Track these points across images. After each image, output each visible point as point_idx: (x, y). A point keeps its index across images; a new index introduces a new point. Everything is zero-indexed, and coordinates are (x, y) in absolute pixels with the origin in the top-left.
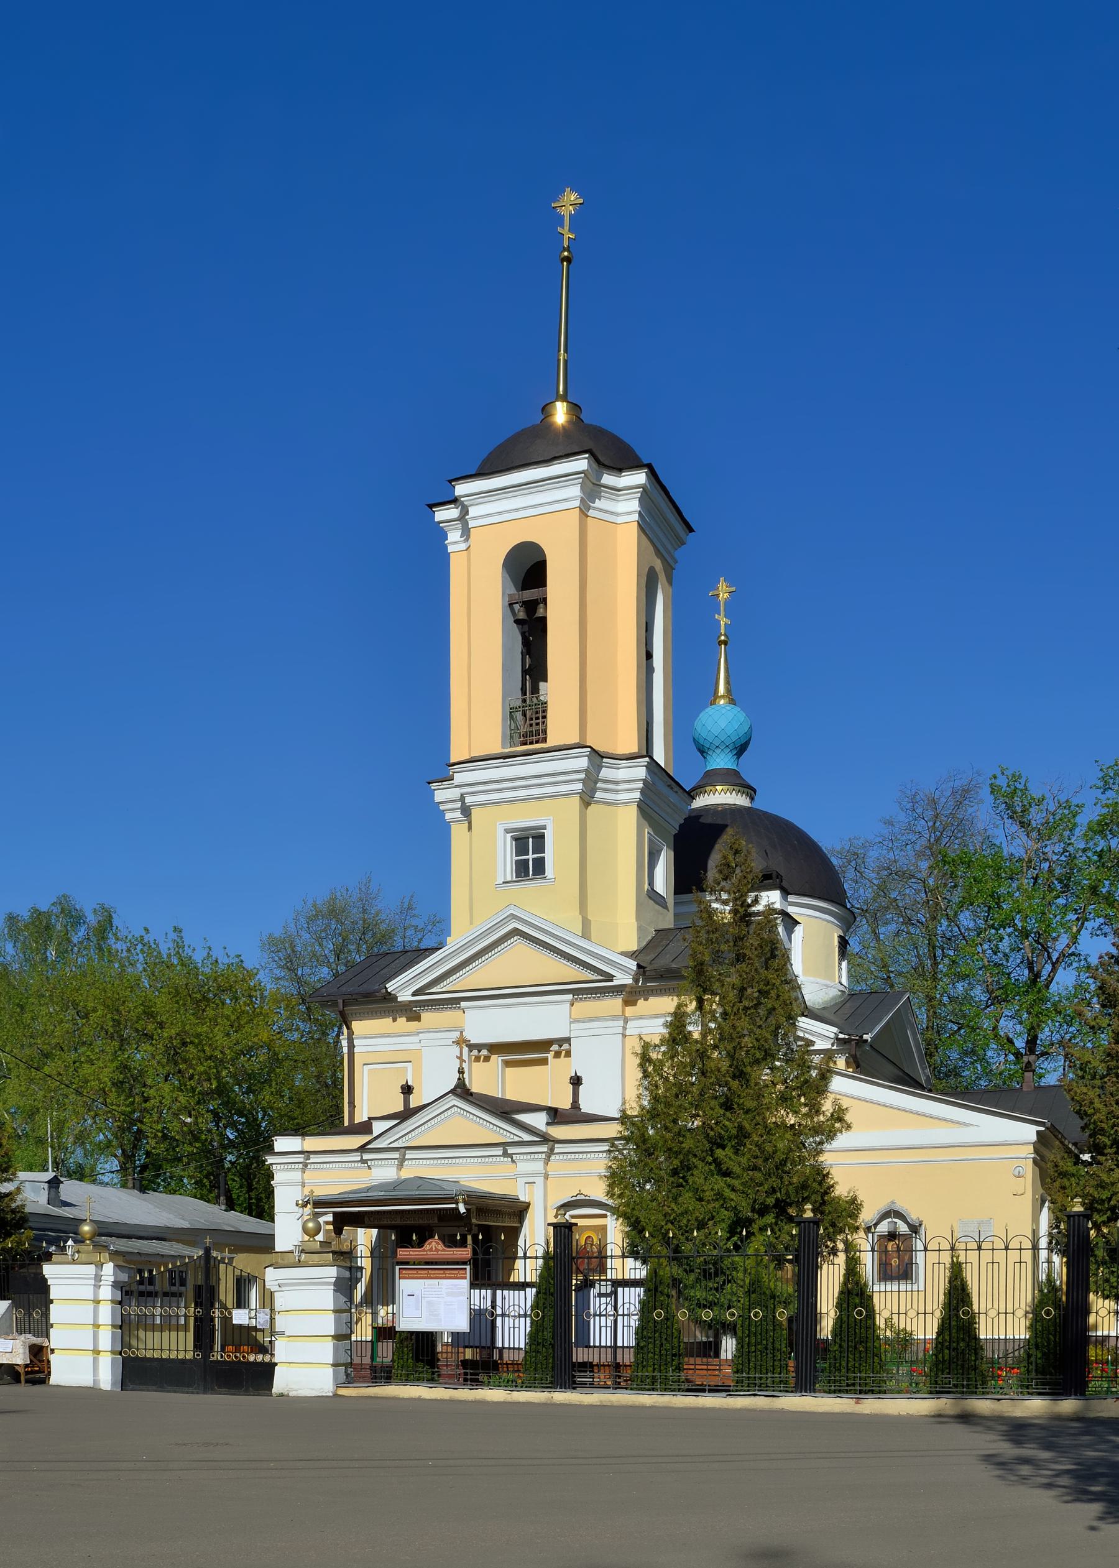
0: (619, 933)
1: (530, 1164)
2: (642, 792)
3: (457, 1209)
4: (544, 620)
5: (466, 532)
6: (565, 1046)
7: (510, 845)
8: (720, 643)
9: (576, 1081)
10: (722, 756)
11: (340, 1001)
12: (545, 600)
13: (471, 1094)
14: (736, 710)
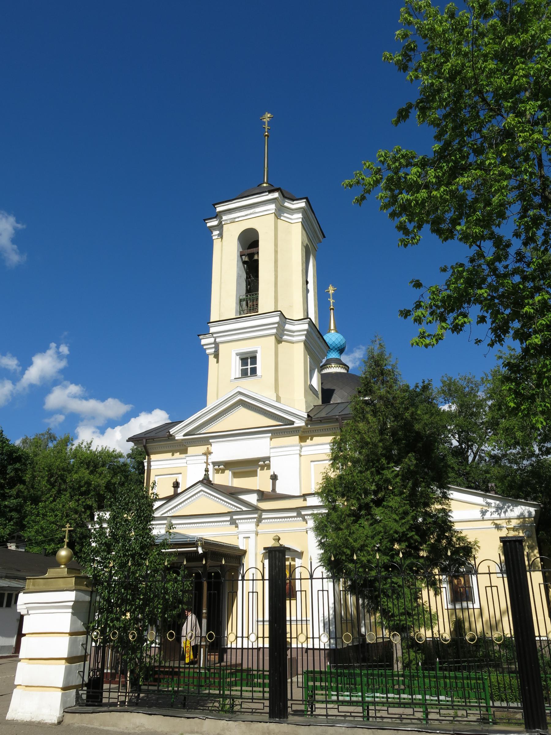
0: (297, 404)
1: (247, 526)
2: (306, 336)
3: (197, 552)
4: (257, 261)
5: (221, 235)
6: (267, 462)
7: (238, 362)
8: (331, 309)
9: (274, 478)
10: (334, 353)
11: (144, 440)
12: (258, 253)
13: (212, 484)
14: (339, 335)
